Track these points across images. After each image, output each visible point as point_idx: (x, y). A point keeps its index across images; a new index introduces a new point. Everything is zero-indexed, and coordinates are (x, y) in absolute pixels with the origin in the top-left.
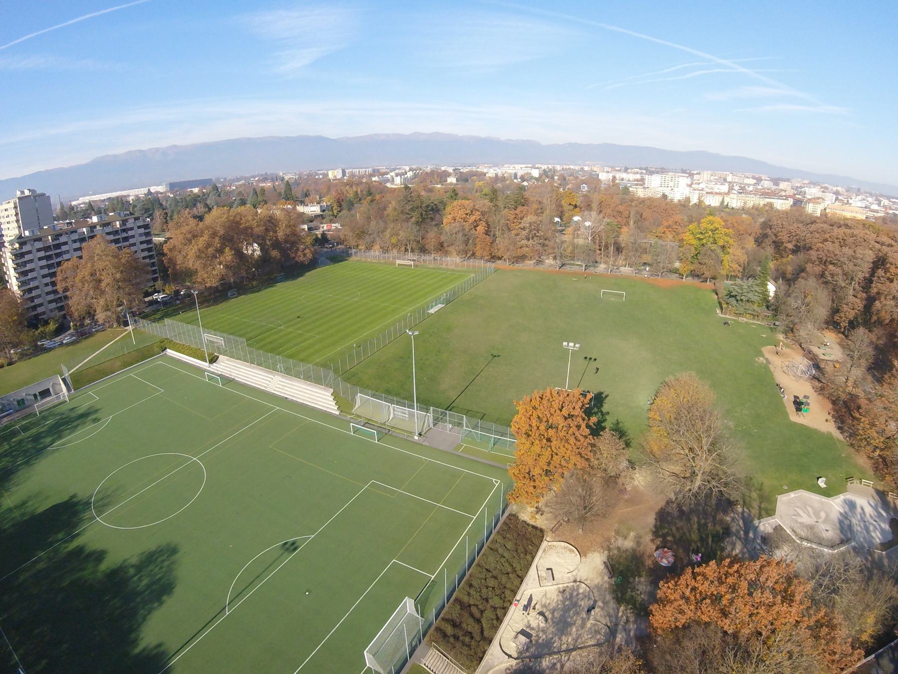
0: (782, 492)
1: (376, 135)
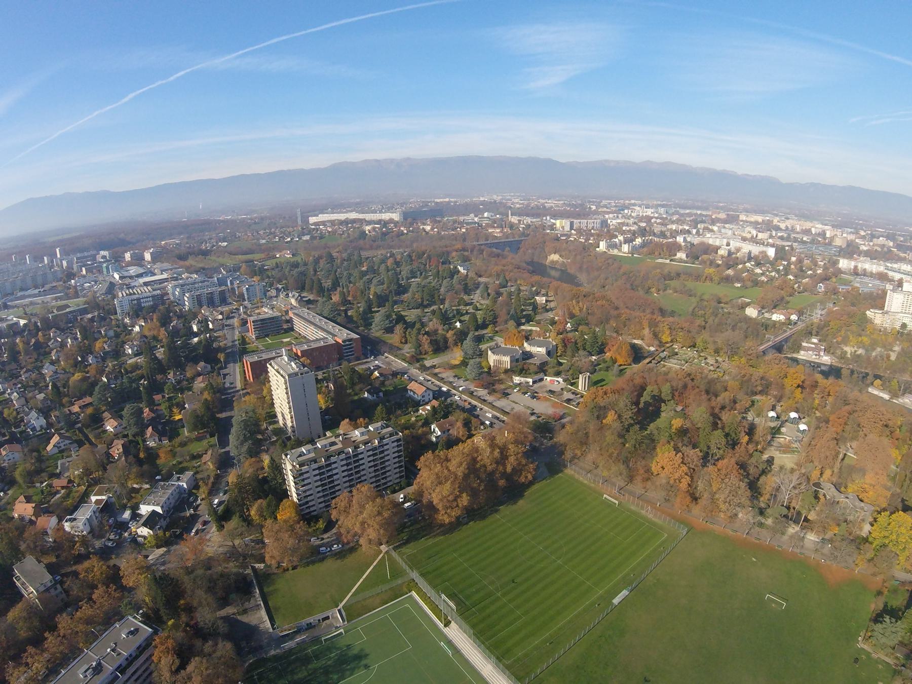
1: (606, 161)
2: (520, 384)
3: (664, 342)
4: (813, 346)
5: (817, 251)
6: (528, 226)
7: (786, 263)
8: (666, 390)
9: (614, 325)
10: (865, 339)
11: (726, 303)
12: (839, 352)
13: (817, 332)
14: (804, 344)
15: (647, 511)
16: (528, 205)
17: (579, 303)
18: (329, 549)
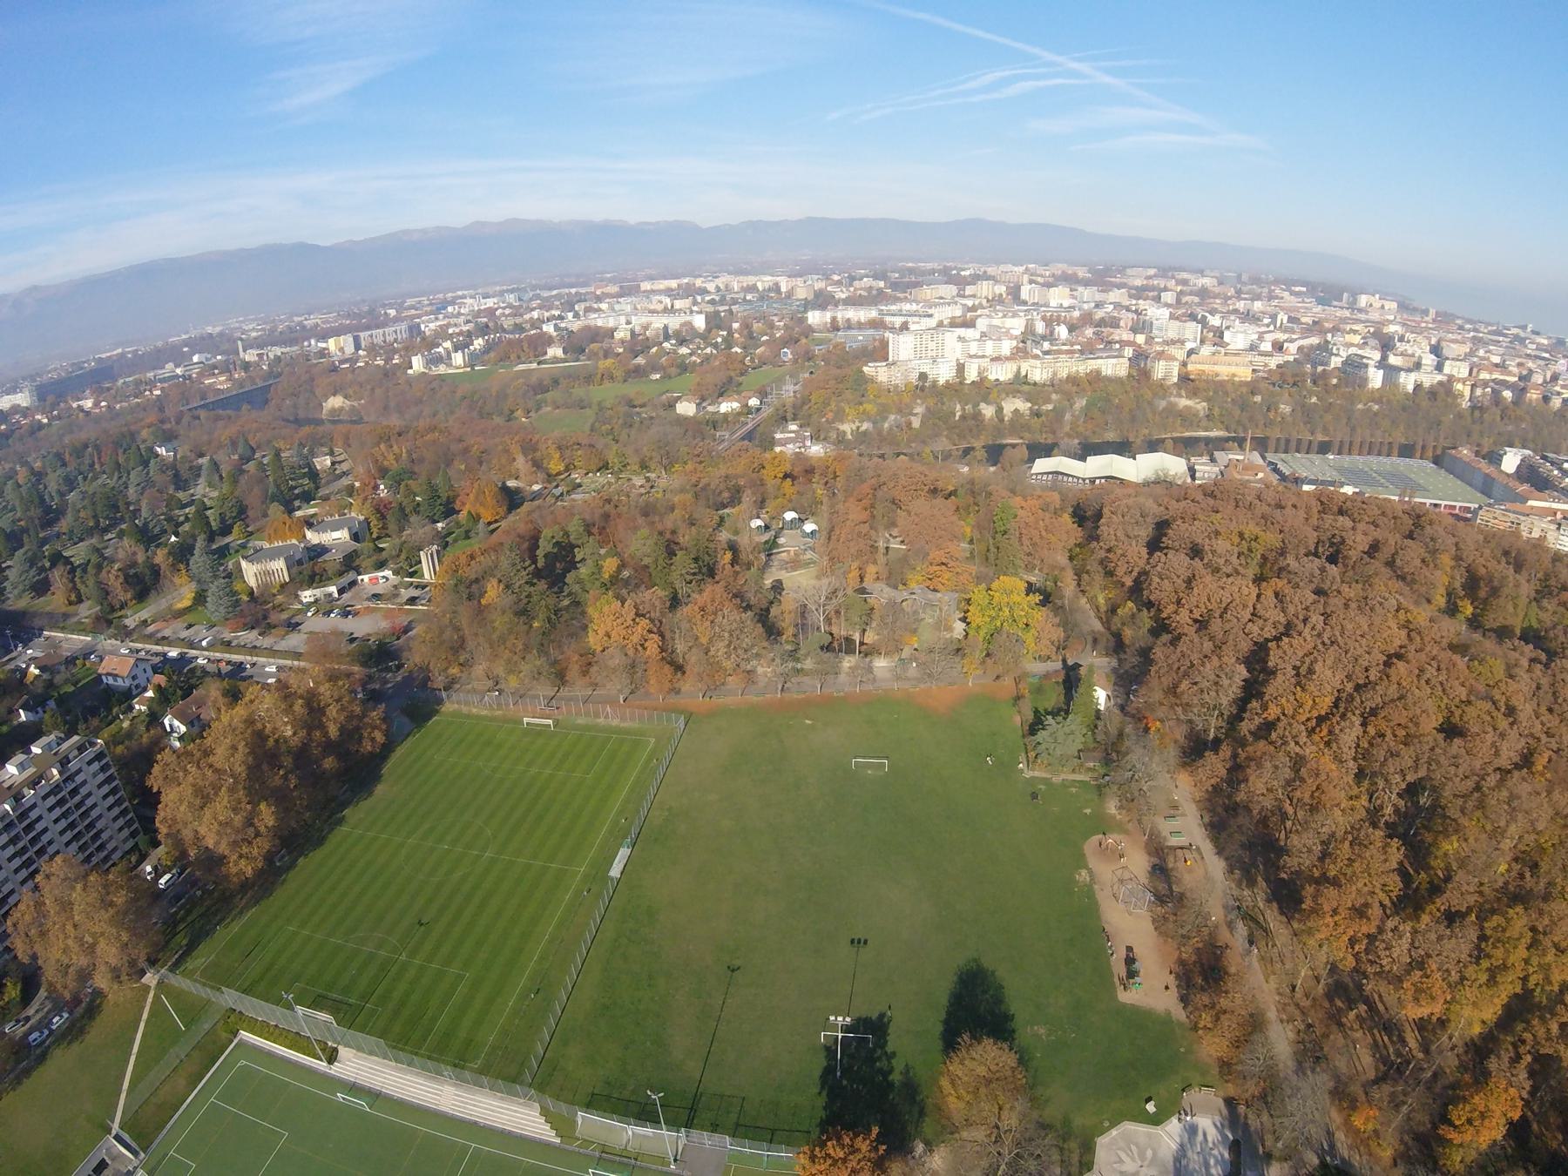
1: (405, 232)
2: (316, 601)
3: (554, 473)
4: (793, 435)
5: (771, 310)
6: (278, 359)
7: (725, 333)
8: (575, 527)
9: (463, 467)
10: (868, 407)
11: (641, 406)
12: (833, 435)
13: (794, 414)
14: (778, 436)
16: (272, 331)
17: (391, 447)
18: (46, 1032)
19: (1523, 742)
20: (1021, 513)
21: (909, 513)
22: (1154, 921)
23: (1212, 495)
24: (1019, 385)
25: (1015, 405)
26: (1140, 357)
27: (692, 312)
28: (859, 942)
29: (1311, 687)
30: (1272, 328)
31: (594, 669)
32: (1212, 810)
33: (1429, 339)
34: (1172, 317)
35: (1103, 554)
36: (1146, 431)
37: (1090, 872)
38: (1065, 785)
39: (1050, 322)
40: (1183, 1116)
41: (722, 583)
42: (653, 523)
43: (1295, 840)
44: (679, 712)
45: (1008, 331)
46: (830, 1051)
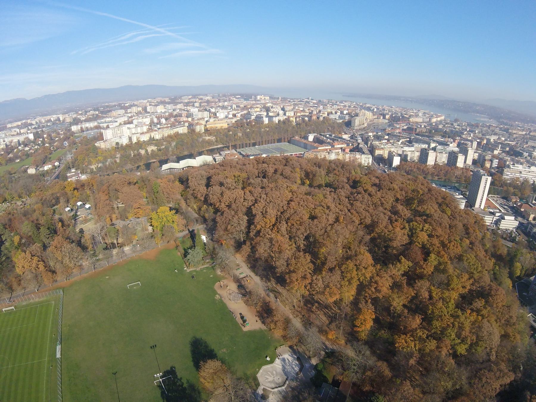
0: (258, 372)
4: (74, 173)
10: (100, 158)
11: (14, 174)
12: (89, 170)
15: (33, 299)
19: (334, 215)
20: (161, 184)
21: (122, 193)
22: (244, 302)
23: (223, 166)
24: (152, 141)
25: (151, 148)
26: (191, 125)
27: (28, 133)
28: (153, 346)
29: (268, 217)
30: (231, 110)
31: (22, 282)
32: (250, 263)
33: (280, 106)
34: (199, 111)
35: (192, 192)
36: (197, 149)
37: (219, 294)
38: (202, 270)
39: (158, 118)
40: (279, 357)
41: (61, 235)
42: (29, 218)
43: (278, 263)
44: (59, 288)
45: (145, 123)
46: (160, 386)
